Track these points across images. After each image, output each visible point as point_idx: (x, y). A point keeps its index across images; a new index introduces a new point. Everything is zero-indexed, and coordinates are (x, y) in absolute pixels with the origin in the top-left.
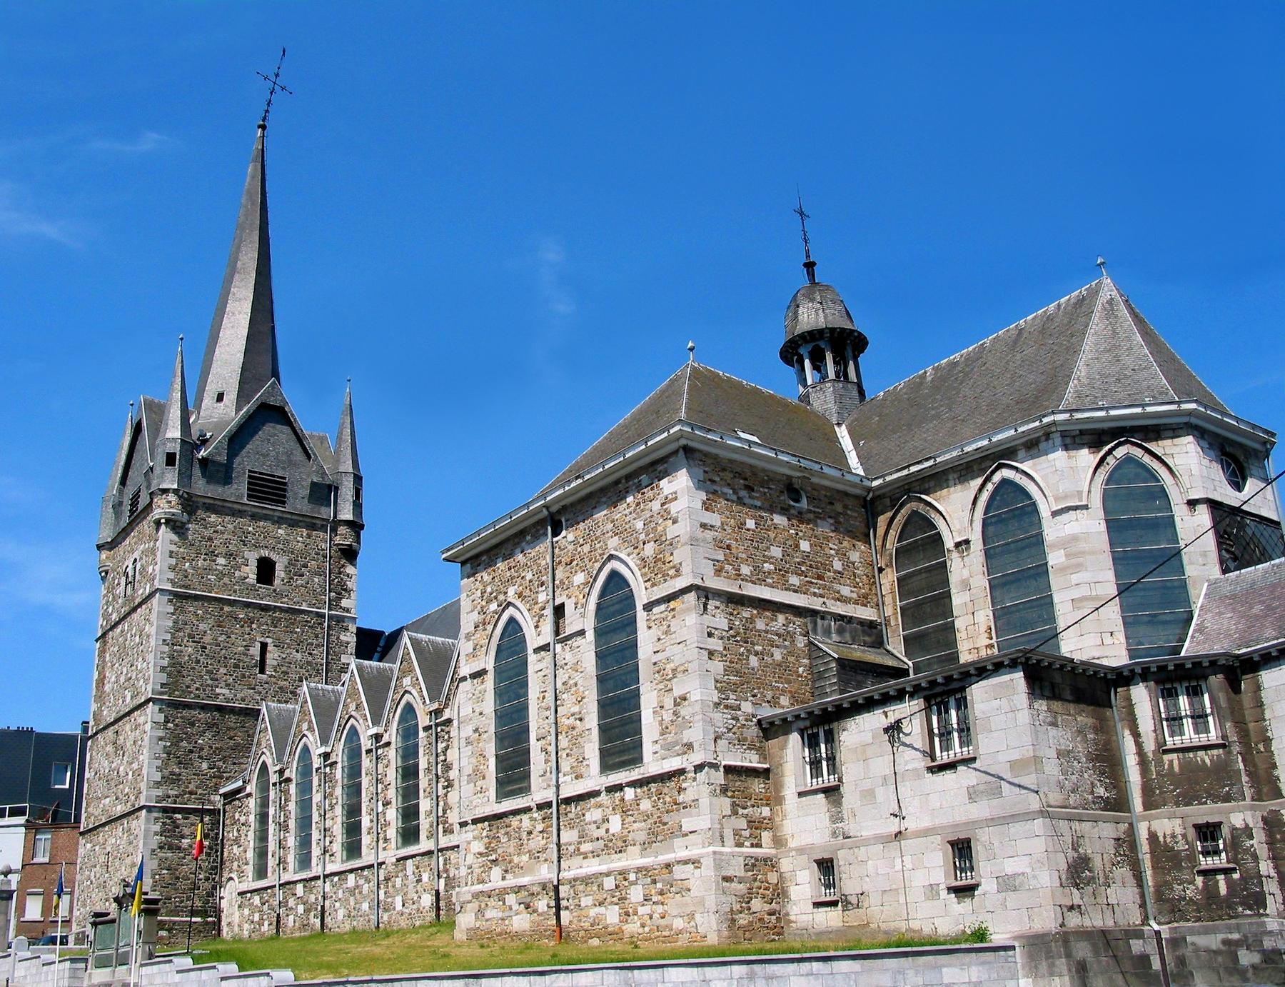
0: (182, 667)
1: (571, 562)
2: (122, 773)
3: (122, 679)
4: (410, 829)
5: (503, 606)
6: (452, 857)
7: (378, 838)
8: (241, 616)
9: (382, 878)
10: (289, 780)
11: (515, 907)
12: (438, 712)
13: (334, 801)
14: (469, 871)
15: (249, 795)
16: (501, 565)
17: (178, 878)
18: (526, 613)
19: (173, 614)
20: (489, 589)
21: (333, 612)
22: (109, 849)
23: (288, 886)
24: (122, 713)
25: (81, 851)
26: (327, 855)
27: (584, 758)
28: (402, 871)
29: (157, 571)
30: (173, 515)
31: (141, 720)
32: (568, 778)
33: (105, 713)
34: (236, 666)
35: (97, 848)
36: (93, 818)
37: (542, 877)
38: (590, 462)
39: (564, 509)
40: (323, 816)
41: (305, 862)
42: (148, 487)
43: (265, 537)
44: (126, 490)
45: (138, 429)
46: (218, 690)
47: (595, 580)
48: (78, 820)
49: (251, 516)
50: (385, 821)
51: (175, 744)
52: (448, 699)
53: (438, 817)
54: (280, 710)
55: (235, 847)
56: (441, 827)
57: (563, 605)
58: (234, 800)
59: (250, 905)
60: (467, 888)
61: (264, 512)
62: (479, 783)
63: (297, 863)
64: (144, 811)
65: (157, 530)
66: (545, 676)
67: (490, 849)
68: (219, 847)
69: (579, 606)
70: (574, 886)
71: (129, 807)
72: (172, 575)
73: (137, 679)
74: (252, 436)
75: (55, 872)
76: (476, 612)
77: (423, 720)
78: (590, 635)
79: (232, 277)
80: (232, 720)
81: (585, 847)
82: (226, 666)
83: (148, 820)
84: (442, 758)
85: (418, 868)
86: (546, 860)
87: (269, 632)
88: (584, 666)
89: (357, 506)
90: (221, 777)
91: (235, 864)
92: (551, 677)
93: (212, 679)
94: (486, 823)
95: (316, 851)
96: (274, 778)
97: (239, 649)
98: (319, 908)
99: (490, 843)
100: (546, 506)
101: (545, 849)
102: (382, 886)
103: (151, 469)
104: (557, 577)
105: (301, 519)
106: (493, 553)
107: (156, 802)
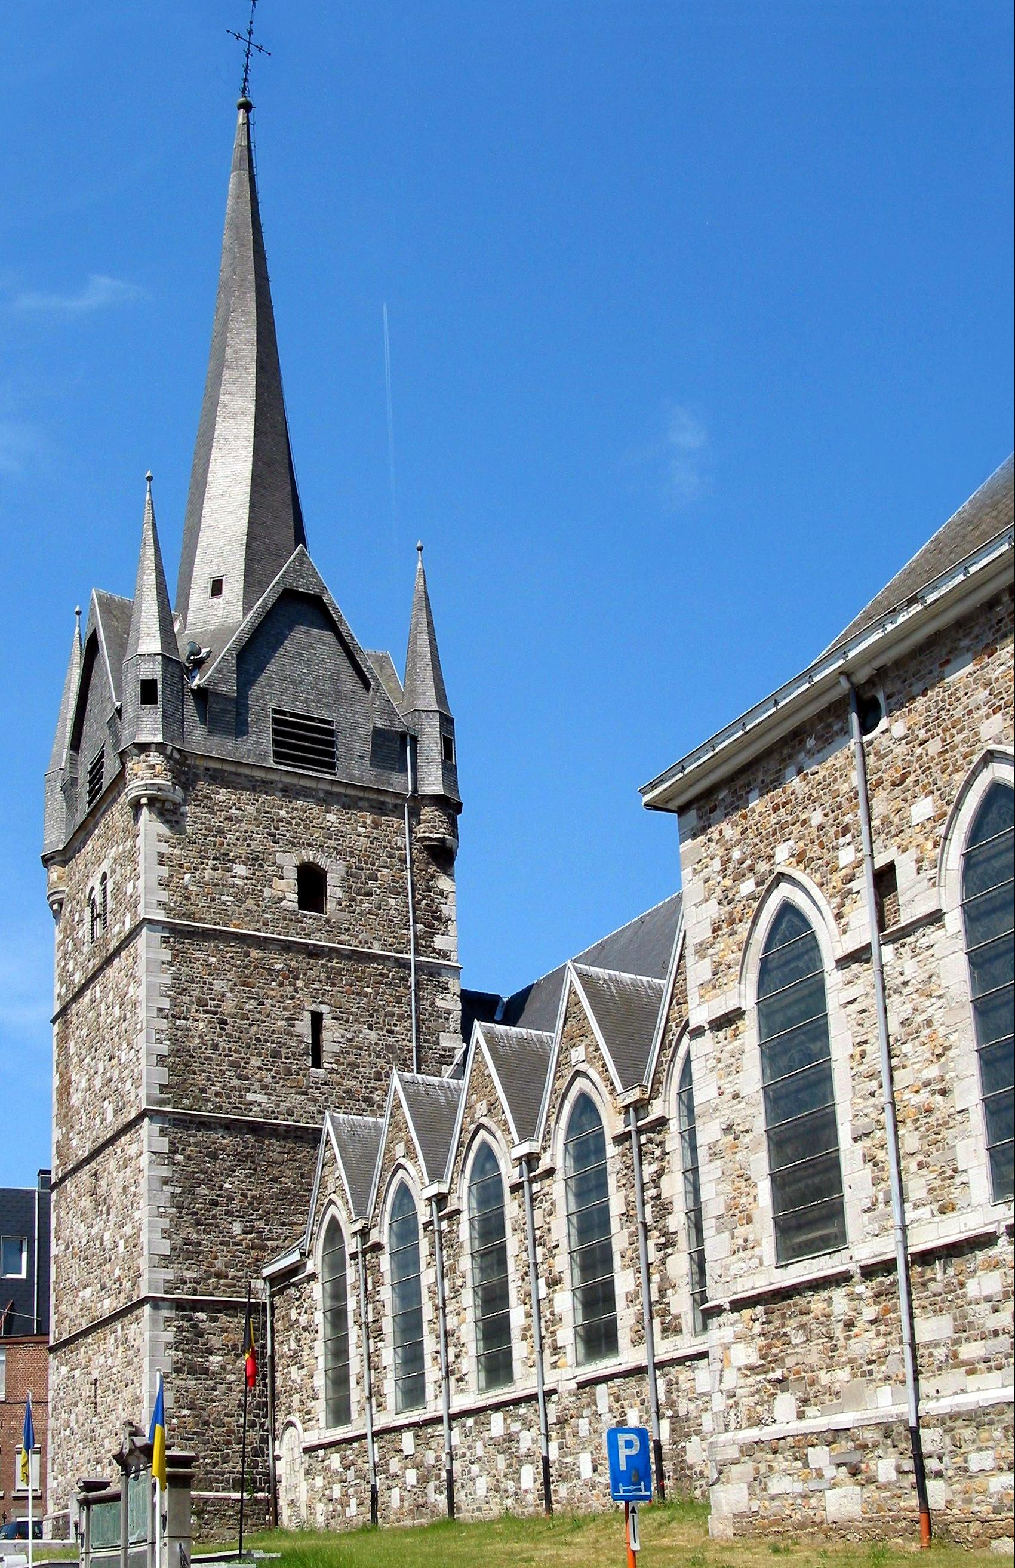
0: (192, 1057)
1: (904, 777)
2: (108, 1244)
3: (98, 1082)
4: (598, 1327)
5: (768, 882)
6: (682, 1378)
7: (541, 1345)
8: (278, 966)
9: (552, 1419)
10: (377, 1247)
11: (830, 1472)
12: (640, 1107)
13: (459, 1282)
14: (731, 1402)
15: (313, 1277)
16: (758, 804)
17: (206, 1423)
18: (815, 892)
19: (170, 963)
20: (736, 854)
21: (422, 958)
22: (95, 1374)
23: (387, 1437)
24: (101, 1141)
25: (53, 1379)
26: (452, 1379)
27: (956, 1171)
28: (589, 1405)
29: (141, 890)
30: (159, 789)
31: (132, 1150)
32: (924, 1212)
33: (74, 1143)
34: (276, 1054)
35: (77, 1373)
36: (67, 1322)
37: (881, 1412)
38: (932, 574)
39: (881, 675)
40: (441, 1308)
41: (413, 1393)
42: (117, 742)
43: (307, 828)
44: (81, 758)
45: (92, 648)
46: (250, 1097)
47: (957, 808)
48: (44, 1330)
49: (282, 790)
50: (552, 1314)
51: (189, 1191)
52: (657, 1081)
53: (651, 1304)
54: (353, 1126)
55: (294, 1369)
56: (657, 1321)
57: (891, 867)
58: (288, 1287)
59: (324, 1469)
60: (729, 1436)
61: (304, 782)
62: (741, 1231)
63: (400, 1394)
64: (147, 1308)
65: (136, 817)
66: (863, 1011)
67: (769, 1360)
68: (268, 1370)
69: (926, 864)
70: (952, 1430)
71: (123, 1301)
72: (164, 896)
73: (122, 1081)
74: (275, 649)
75: (16, 1416)
76: (714, 902)
77: (613, 1124)
78: (954, 921)
79: (219, 376)
80: (275, 1149)
81: (970, 1351)
82: (259, 1055)
83: (154, 1322)
84: (652, 1192)
85: (617, 1400)
86: (887, 1378)
87: (323, 995)
88: (944, 984)
89: (449, 770)
90: (264, 1248)
91: (296, 1397)
92: (876, 1009)
93: (239, 1077)
94: (760, 1309)
95: (432, 1373)
96: (352, 1245)
97: (279, 1023)
98: (444, 1474)
99: (769, 1347)
100: (845, 673)
101: (882, 1357)
102: (554, 1434)
103: (119, 712)
104: (875, 813)
105: (361, 794)
106: (740, 782)
107: (166, 1292)
